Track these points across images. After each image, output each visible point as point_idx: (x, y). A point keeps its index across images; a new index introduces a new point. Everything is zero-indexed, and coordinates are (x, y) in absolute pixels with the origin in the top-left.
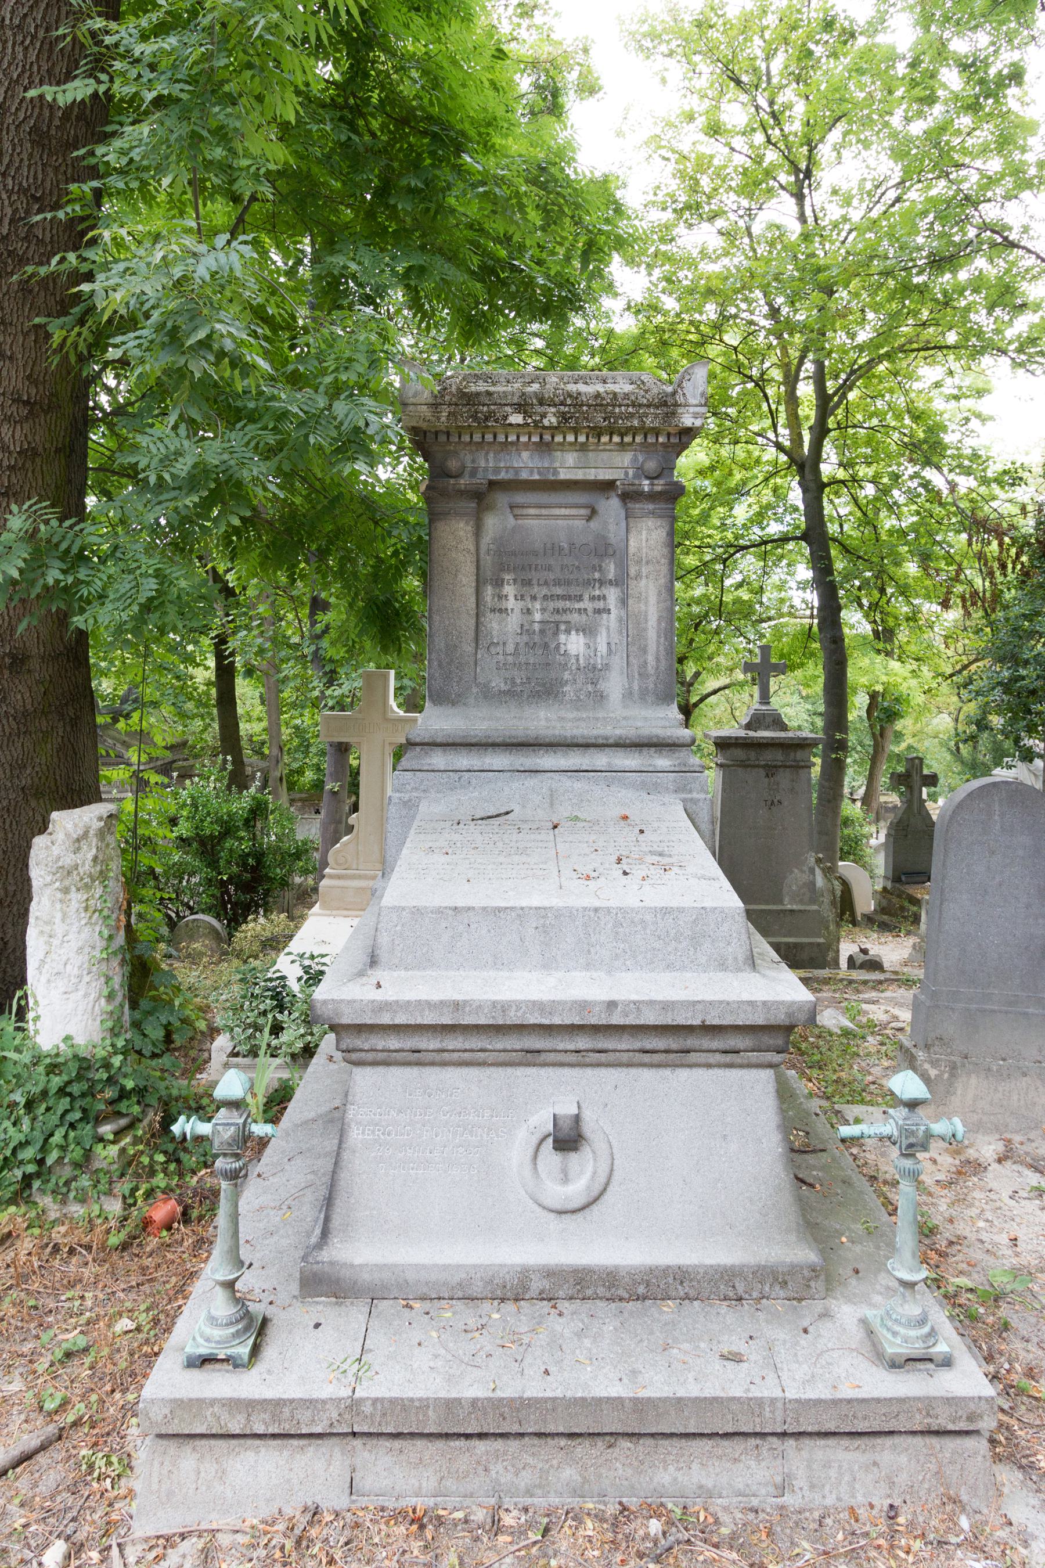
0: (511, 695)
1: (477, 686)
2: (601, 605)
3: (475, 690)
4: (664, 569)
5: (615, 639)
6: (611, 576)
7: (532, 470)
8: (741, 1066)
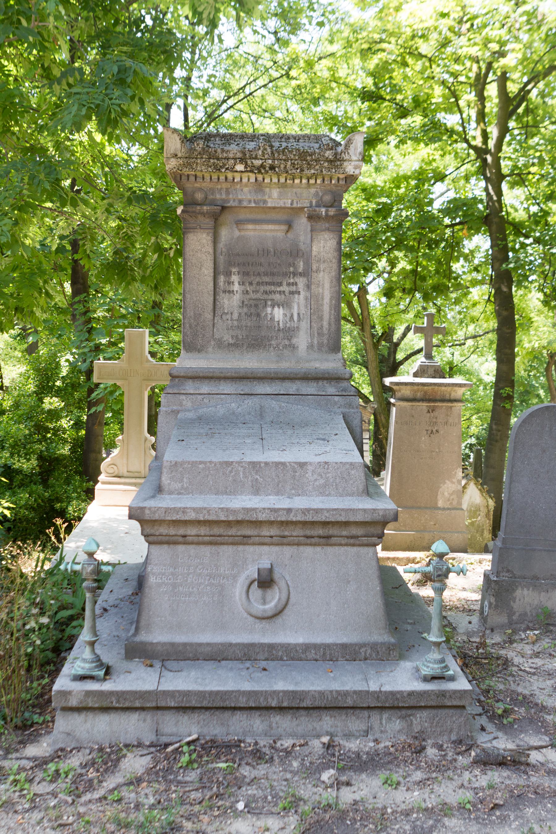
0: (235, 346)
1: (214, 340)
2: (294, 288)
3: (213, 343)
4: (335, 266)
5: (303, 311)
6: (300, 270)
7: (250, 201)
8: (360, 545)
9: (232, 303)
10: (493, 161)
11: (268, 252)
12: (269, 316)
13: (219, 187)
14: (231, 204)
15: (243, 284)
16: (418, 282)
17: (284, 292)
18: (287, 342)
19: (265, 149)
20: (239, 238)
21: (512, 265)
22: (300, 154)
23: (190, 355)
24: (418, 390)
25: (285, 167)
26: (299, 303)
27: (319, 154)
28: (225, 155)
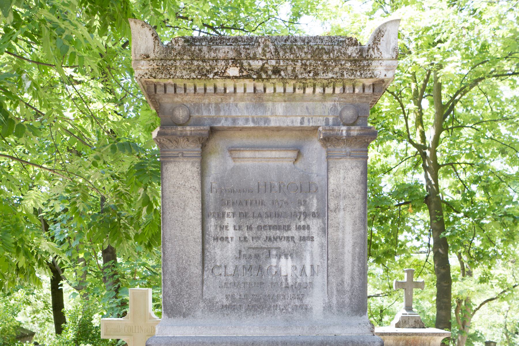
0: (231, 308)
1: (204, 301)
2: (305, 233)
3: (202, 305)
5: (317, 262)
9: (226, 252)
10: (431, 154)
11: (272, 187)
12: (274, 270)
13: (206, 101)
14: (223, 123)
15: (240, 228)
16: (372, 249)
17: (293, 238)
18: (297, 303)
19: (267, 46)
20: (233, 169)
21: (448, 234)
22: (314, 52)
23: (173, 320)
24: (401, 339)
25: (294, 70)
26: (313, 253)
27: (339, 51)
28: (213, 55)
